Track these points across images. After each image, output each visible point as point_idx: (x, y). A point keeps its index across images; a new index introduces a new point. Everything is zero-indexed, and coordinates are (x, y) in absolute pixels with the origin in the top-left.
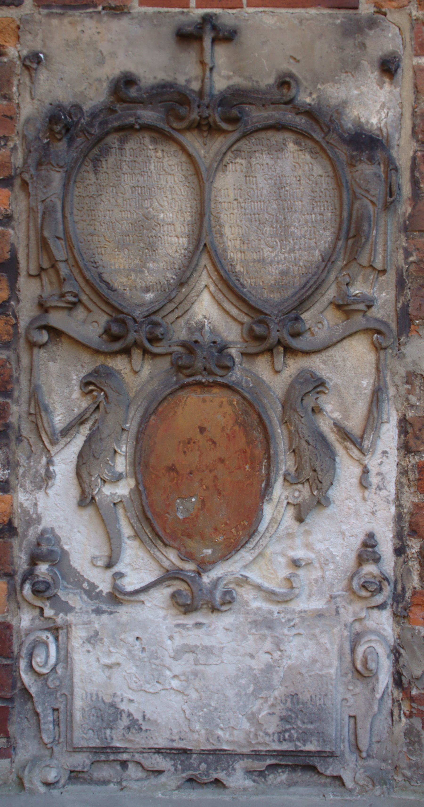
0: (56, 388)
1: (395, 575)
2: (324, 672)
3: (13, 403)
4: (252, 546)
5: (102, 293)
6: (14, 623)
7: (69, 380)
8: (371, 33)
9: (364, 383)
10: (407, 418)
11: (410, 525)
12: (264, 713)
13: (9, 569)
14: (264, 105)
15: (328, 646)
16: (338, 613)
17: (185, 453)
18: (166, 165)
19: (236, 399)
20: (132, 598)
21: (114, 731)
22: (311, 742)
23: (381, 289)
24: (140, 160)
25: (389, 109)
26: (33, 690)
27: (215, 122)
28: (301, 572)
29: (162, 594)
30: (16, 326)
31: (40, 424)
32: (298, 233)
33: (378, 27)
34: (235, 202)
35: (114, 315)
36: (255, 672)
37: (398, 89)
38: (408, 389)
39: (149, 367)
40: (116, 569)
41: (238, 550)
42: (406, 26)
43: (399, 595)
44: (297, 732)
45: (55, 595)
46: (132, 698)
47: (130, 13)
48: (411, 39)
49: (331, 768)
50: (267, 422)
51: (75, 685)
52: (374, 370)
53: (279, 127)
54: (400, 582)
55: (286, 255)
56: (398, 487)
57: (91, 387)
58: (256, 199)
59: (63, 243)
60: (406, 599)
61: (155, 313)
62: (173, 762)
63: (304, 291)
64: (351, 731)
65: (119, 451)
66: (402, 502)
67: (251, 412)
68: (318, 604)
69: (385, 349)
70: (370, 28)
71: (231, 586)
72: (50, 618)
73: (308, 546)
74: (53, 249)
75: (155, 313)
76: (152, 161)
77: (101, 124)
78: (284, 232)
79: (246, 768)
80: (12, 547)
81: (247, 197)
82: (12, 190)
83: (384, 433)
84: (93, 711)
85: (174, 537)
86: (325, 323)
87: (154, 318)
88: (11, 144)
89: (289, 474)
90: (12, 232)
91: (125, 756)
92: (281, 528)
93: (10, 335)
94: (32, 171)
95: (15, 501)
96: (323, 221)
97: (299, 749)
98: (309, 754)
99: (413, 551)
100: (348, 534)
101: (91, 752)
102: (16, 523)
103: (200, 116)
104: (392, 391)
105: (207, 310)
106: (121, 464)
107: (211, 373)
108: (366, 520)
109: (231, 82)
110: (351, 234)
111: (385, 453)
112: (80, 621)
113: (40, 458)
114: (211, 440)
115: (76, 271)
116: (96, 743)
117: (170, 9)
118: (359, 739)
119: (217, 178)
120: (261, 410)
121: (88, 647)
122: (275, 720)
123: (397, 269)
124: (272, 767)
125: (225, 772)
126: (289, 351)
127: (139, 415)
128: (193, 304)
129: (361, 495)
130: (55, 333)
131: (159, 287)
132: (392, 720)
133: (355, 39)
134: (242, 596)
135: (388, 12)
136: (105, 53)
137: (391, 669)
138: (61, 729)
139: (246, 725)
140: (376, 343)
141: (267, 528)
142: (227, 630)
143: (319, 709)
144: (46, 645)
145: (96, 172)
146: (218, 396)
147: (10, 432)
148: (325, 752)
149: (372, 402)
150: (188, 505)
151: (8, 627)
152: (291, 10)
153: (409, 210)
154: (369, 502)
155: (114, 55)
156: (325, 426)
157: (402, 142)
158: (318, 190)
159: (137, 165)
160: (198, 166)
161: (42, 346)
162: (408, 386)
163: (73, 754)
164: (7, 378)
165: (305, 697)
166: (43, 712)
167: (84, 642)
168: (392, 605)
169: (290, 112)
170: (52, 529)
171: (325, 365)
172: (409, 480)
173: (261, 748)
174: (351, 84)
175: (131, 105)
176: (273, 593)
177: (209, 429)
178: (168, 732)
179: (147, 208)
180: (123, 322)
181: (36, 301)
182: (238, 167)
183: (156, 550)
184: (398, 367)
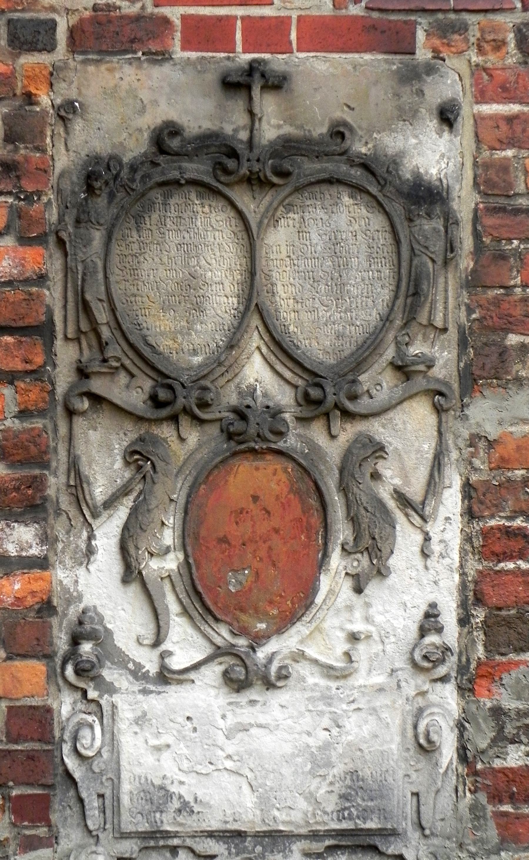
0: (97, 458)
1: (459, 646)
2: (385, 747)
3: (50, 475)
4: (308, 620)
5: (145, 359)
6: (55, 706)
7: (110, 449)
8: (429, 79)
9: (426, 447)
10: (471, 482)
11: (475, 594)
12: (322, 791)
13: (48, 650)
14: (317, 157)
15: (389, 720)
16: (399, 687)
17: (237, 523)
18: (213, 221)
19: (290, 466)
20: (181, 677)
21: (164, 815)
22: (372, 819)
23: (442, 348)
24: (185, 215)
25: (449, 158)
26: (77, 775)
27: (265, 177)
28: (361, 647)
29: (213, 672)
30: (52, 392)
31: (81, 496)
32: (354, 291)
33: (436, 73)
34: (288, 259)
35: (159, 379)
36: (312, 750)
37: (459, 138)
38: (472, 453)
39: (198, 434)
40: (163, 647)
41: (294, 623)
42: (466, 71)
43: (464, 666)
44: (357, 809)
45: (100, 676)
46: (183, 779)
47: (172, 58)
48: (471, 85)
49: (392, 847)
50: (323, 489)
51: (122, 768)
52: (436, 433)
53: (331, 181)
54: (464, 653)
55: (342, 314)
56: (463, 555)
57: (136, 457)
58: (309, 255)
59: (105, 305)
60: (471, 670)
61: (204, 377)
62: (226, 846)
63: (361, 351)
64: (414, 808)
65: (166, 523)
66: (466, 570)
67: (307, 479)
68: (379, 679)
69: (447, 410)
70: (428, 75)
71: (287, 662)
72: (93, 701)
73: (368, 619)
74: (96, 313)
75: (204, 377)
76: (198, 217)
77: (143, 177)
78: (339, 288)
79: (304, 850)
80: (51, 627)
81: (300, 253)
82: (46, 248)
83: (447, 499)
84: (142, 794)
85: (225, 609)
86: (384, 384)
87: (203, 382)
88: (45, 199)
89: (348, 544)
90: (47, 293)
91: (176, 842)
92: (339, 600)
93: (46, 402)
94: (71, 229)
95: (54, 579)
96: (379, 279)
97: (359, 827)
98: (370, 832)
99: (478, 620)
100: (409, 605)
101: (139, 838)
102: (55, 602)
103: (250, 171)
104: (454, 455)
105: (257, 373)
106: (168, 537)
107: (265, 440)
108: (429, 590)
109: (282, 132)
110: (411, 292)
111: (448, 519)
112: (126, 700)
113: (81, 532)
114: (265, 509)
115: (118, 334)
116: (144, 827)
117: (214, 54)
118: (421, 815)
119: (268, 234)
120: (318, 477)
121: (136, 729)
122: (334, 798)
123: (459, 326)
124: (331, 849)
125: (281, 854)
126: (348, 415)
127: (187, 484)
128: (243, 366)
129: (423, 563)
130: (97, 400)
131: (207, 351)
132: (457, 797)
133: (412, 85)
134: (298, 672)
135: (446, 57)
136: (145, 102)
137: (456, 744)
138: (107, 815)
139: (302, 804)
140: (437, 405)
141: (324, 600)
142: (282, 706)
143: (379, 786)
144: (91, 727)
145: (138, 230)
146: (273, 464)
147: (48, 505)
148: (386, 829)
149: (433, 467)
150: (240, 577)
151: (48, 710)
152: (344, 56)
153: (472, 264)
154: (432, 571)
155: (155, 103)
156: (385, 493)
157: (463, 194)
158: (375, 246)
159: (183, 221)
160: (249, 222)
161: (83, 413)
162: (472, 449)
163: (120, 841)
164: (43, 448)
165: (366, 772)
166: (88, 797)
167: (131, 724)
168: (456, 678)
169: (345, 164)
170: (95, 607)
171: (385, 428)
172: (473, 547)
173: (319, 828)
174: (409, 132)
175: (175, 158)
176: (331, 667)
177: (262, 497)
178: (222, 814)
179: (194, 267)
180: (170, 387)
181: (75, 366)
182: (291, 222)
183: (206, 626)
184: (462, 429)
